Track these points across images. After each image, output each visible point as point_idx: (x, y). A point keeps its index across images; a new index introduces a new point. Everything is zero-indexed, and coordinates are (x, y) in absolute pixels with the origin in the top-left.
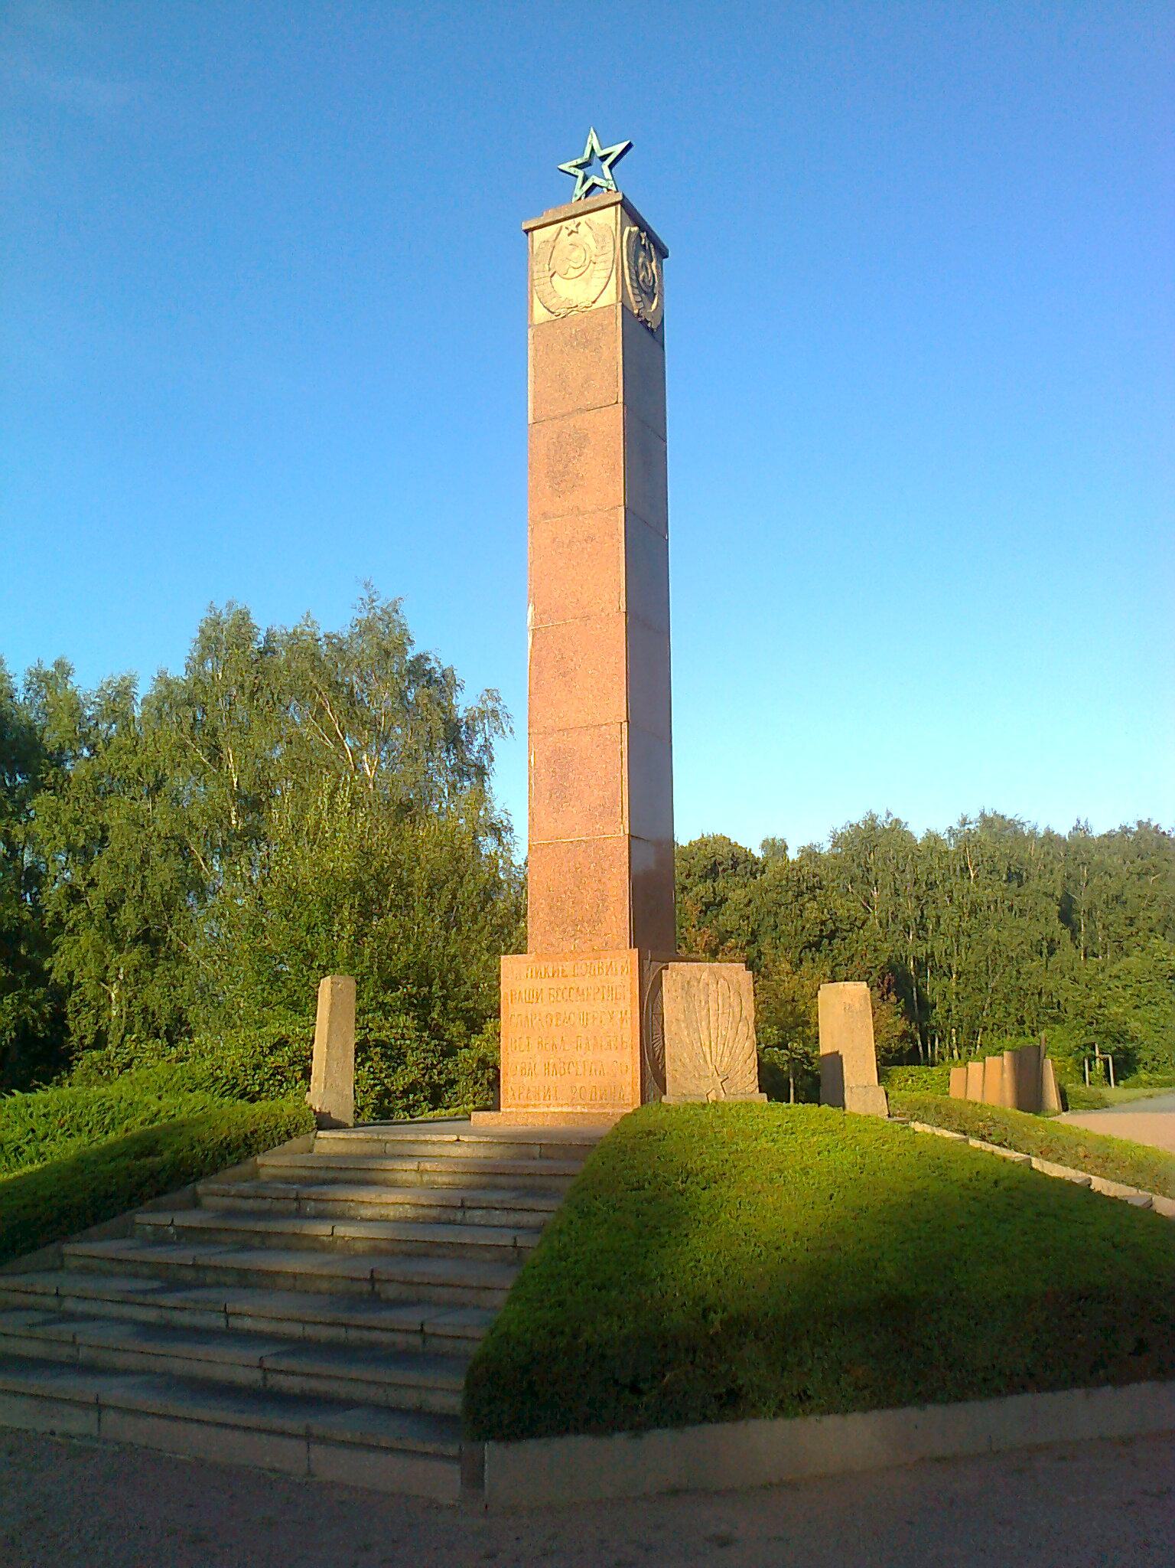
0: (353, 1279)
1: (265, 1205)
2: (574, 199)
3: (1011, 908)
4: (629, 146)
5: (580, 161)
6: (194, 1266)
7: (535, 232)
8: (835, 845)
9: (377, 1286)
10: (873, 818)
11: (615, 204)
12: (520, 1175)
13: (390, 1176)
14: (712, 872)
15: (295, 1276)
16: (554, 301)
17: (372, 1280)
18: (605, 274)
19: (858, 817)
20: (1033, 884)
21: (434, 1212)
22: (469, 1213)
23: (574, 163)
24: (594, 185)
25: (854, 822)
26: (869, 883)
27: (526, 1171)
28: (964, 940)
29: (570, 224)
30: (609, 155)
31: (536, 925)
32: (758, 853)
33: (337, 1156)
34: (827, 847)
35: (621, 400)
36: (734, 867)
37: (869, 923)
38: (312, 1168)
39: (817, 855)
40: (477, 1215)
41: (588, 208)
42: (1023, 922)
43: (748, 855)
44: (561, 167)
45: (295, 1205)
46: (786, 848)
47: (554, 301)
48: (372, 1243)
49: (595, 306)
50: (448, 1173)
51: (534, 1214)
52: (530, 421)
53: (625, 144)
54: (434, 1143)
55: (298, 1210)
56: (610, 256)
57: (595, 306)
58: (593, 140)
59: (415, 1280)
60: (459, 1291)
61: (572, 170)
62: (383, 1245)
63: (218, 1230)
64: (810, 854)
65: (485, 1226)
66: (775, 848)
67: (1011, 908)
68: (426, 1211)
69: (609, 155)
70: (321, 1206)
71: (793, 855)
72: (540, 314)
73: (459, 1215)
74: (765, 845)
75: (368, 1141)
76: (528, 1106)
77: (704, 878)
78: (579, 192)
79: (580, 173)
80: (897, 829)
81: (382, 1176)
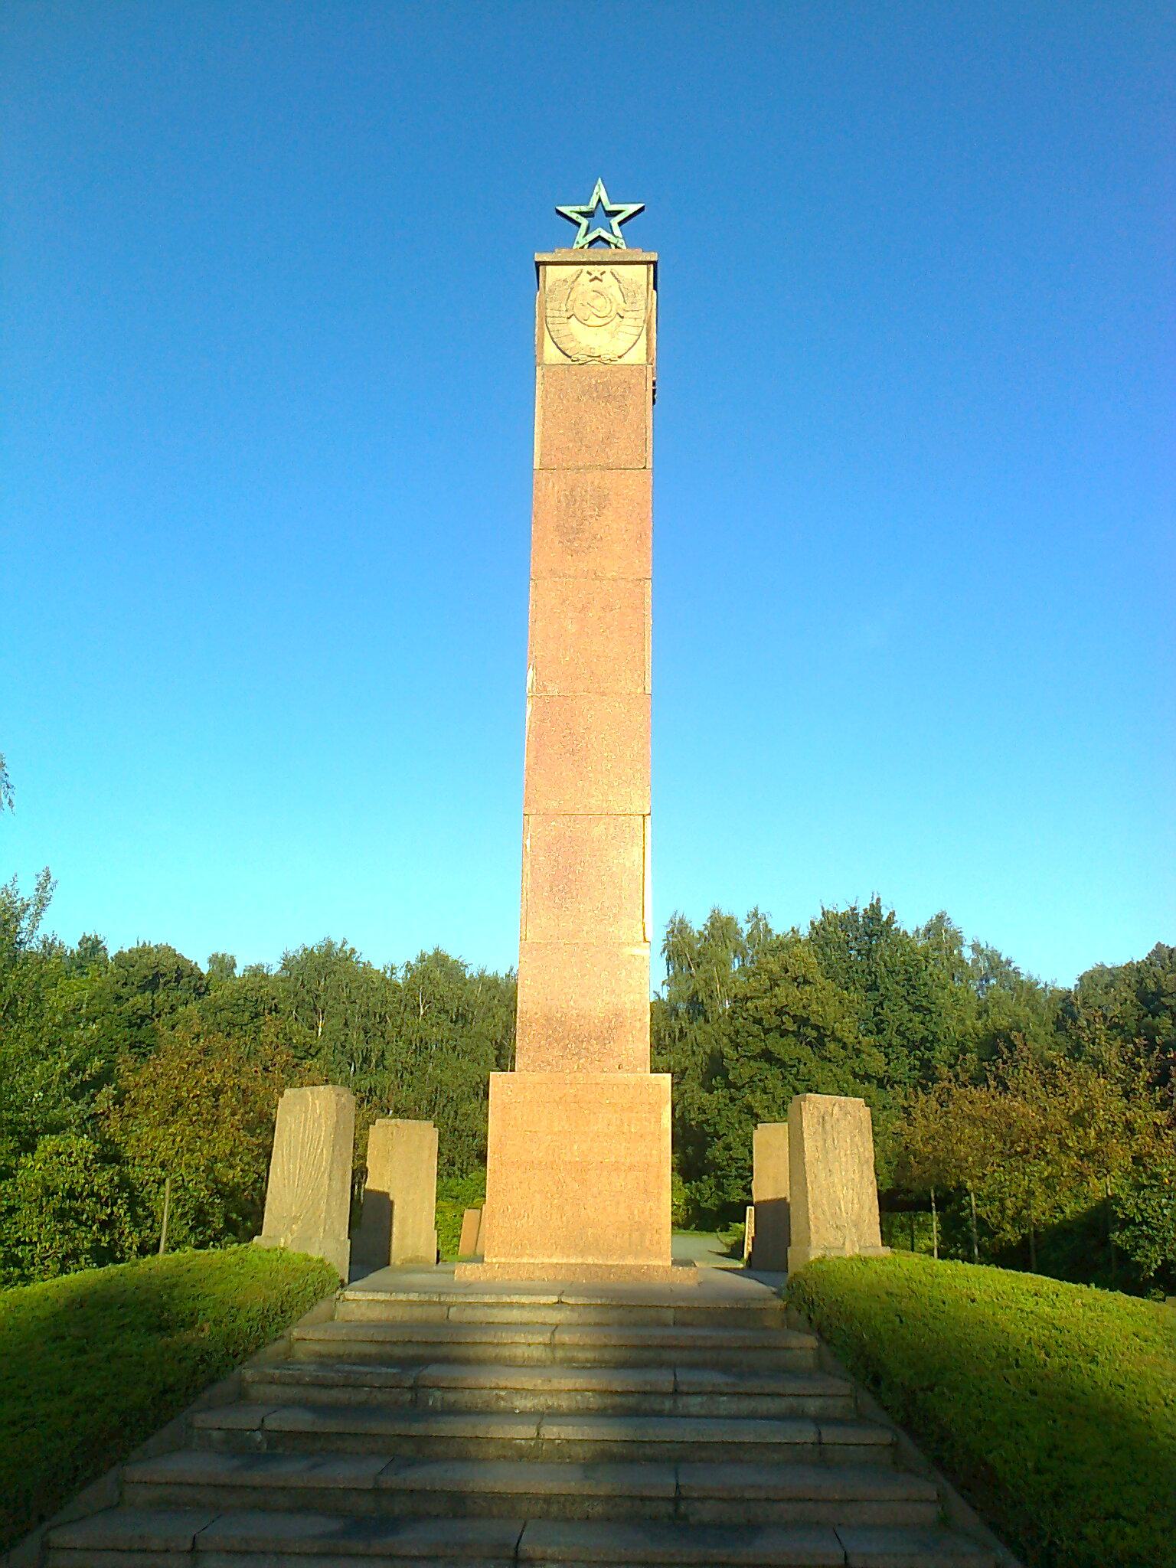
0: (643, 1499)
1: (361, 1396)
2: (575, 246)
3: (454, 1048)
4: (642, 209)
5: (584, 209)
6: (377, 1492)
7: (549, 268)
8: (285, 967)
9: (683, 1507)
10: (330, 945)
11: (648, 263)
12: (700, 1348)
13: (506, 1352)
14: (152, 983)
15: (548, 1499)
16: (572, 345)
17: (677, 1500)
18: (636, 331)
19: (313, 940)
20: (476, 1028)
21: (631, 1401)
22: (682, 1401)
23: (577, 208)
24: (599, 238)
25: (309, 946)
26: (315, 1010)
27: (709, 1343)
28: (407, 1076)
29: (596, 270)
30: (619, 212)
31: (524, 1043)
32: (205, 968)
33: (377, 1325)
34: (275, 969)
35: (649, 466)
36: (177, 980)
37: (324, 1052)
38: (383, 1342)
39: (266, 977)
40: (694, 1404)
41: (617, 259)
42: (465, 1063)
43: (193, 972)
44: (560, 209)
45: (408, 1396)
46: (235, 965)
47: (572, 345)
48: (599, 1447)
49: (620, 361)
50: (594, 1347)
51: (777, 1400)
52: (536, 466)
53: (640, 206)
54: (522, 1306)
55: (414, 1402)
56: (642, 314)
57: (620, 361)
58: (600, 191)
59: (747, 1495)
60: (810, 1505)
61: (574, 216)
62: (616, 1449)
63: (340, 1435)
64: (256, 972)
65: (706, 1417)
66: (223, 965)
67: (454, 1048)
68: (618, 1400)
69: (619, 212)
70: (451, 1397)
71: (238, 972)
72: (551, 354)
73: (668, 1404)
74: (214, 960)
75: (421, 1304)
76: (521, 1256)
77: (143, 989)
78: (581, 240)
79: (584, 222)
80: (348, 957)
81: (492, 1352)
